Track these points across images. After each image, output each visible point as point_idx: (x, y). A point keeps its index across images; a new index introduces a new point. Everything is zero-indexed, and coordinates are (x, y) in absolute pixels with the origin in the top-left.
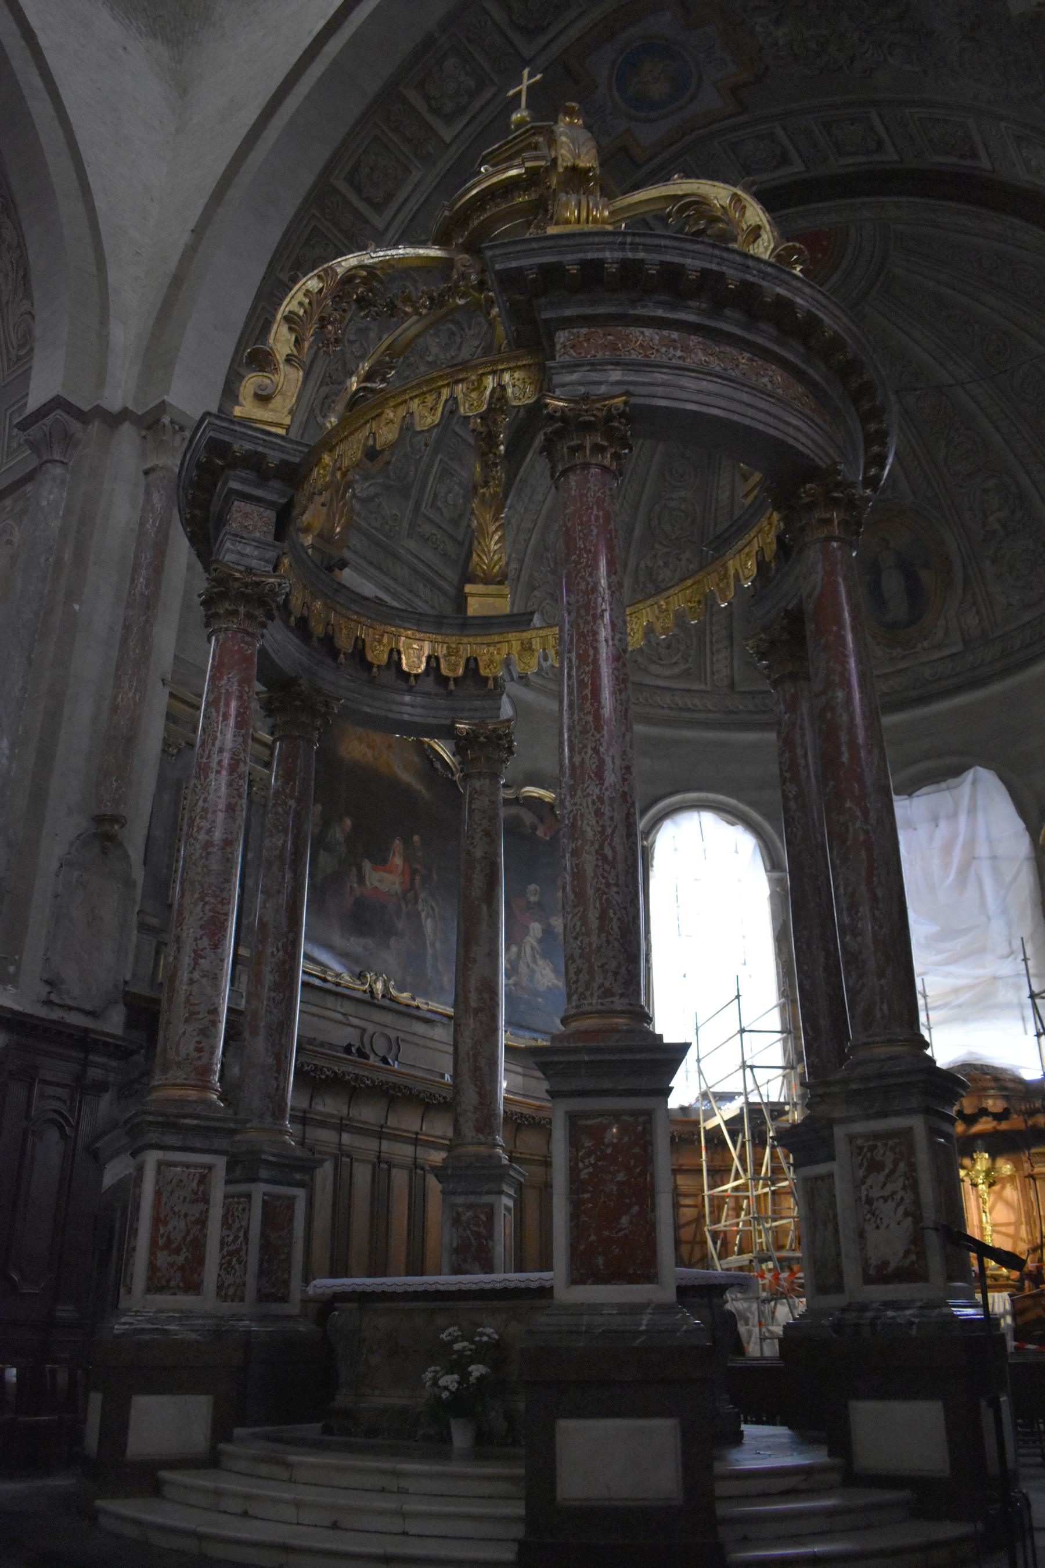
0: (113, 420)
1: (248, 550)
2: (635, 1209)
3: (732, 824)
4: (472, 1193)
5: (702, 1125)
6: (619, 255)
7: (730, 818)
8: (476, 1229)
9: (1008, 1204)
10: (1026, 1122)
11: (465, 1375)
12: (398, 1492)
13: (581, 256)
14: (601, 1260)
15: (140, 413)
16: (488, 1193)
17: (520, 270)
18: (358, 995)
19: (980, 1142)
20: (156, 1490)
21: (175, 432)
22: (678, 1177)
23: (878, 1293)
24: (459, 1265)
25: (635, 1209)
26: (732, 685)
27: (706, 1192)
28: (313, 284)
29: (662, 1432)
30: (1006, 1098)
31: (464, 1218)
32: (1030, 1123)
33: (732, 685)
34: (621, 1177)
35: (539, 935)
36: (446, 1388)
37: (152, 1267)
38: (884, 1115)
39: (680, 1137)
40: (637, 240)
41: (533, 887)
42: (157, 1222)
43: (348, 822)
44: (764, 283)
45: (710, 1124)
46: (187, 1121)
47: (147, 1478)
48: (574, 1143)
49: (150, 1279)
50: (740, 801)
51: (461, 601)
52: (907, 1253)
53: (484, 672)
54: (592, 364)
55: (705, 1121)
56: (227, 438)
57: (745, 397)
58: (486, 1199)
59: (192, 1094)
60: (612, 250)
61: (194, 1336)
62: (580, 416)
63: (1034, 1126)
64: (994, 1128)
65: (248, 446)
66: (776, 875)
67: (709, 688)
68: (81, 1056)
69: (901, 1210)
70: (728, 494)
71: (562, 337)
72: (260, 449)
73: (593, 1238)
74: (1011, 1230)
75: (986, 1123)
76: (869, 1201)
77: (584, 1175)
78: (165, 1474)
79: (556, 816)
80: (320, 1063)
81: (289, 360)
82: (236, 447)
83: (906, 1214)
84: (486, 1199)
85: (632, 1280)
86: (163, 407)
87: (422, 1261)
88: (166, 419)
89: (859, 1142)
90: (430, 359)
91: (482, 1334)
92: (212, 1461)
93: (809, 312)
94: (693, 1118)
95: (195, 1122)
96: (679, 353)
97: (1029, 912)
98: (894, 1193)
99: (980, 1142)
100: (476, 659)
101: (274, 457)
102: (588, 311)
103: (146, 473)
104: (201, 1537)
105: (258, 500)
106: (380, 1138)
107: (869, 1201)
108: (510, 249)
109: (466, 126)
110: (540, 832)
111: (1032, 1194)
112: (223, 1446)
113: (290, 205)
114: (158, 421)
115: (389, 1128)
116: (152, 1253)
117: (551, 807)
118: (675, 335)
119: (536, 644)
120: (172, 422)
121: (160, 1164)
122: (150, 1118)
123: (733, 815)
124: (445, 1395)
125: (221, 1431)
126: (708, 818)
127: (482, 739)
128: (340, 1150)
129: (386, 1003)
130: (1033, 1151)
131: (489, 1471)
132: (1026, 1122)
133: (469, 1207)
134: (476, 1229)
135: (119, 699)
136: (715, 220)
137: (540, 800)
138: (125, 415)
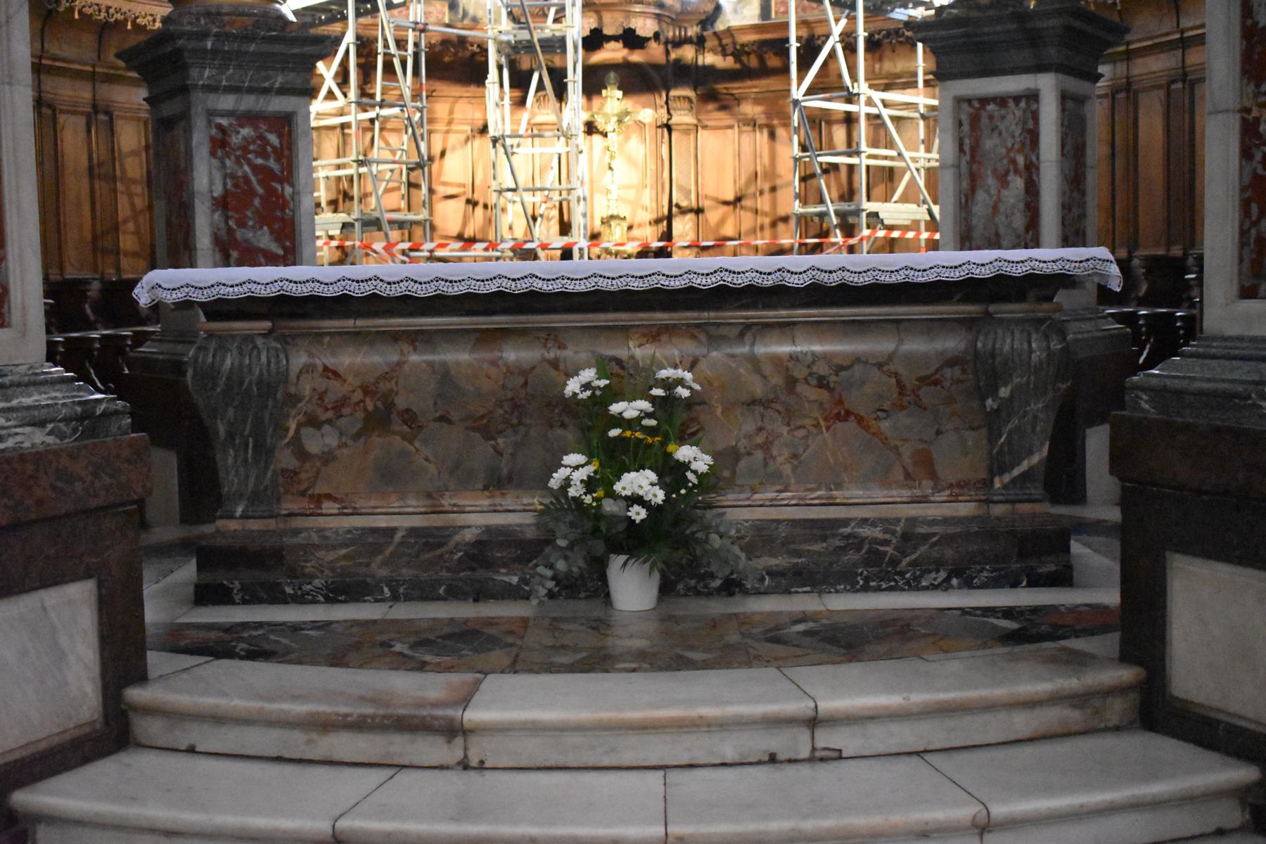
4: (251, 90)
8: (259, 161)
9: (631, 161)
10: (668, 53)
12: (811, 760)
16: (283, 91)
19: (612, 75)
24: (230, 231)
30: (658, 17)
31: (235, 140)
32: (673, 56)
36: (637, 500)
58: (278, 104)
61: (38, 438)
63: (678, 61)
64: (624, 58)
74: (631, 194)
75: (613, 50)
84: (278, 104)
87: (58, 214)
91: (669, 385)
92: (113, 733)
99: (612, 75)
111: (665, 150)
112: (136, 694)
130: (673, 93)
132: (668, 53)
133: (250, 118)
134: (259, 161)
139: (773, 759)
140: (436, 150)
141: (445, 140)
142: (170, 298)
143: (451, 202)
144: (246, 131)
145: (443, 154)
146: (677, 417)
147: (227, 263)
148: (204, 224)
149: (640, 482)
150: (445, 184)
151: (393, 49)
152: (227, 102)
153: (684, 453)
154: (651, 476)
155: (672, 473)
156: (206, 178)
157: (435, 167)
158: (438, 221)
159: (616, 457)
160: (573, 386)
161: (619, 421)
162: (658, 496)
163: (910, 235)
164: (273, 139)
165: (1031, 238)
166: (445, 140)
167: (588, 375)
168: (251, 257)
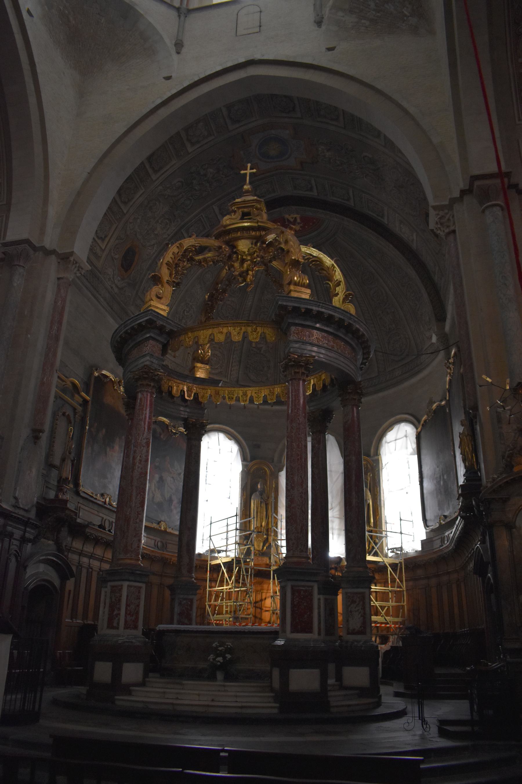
0: (48, 253)
1: (154, 361)
2: (308, 613)
3: (230, 439)
5: (209, 562)
6: (317, 309)
7: (230, 437)
11: (224, 658)
13: (306, 306)
14: (299, 627)
15: (60, 252)
17: (287, 306)
18: (100, 503)
20: (130, 693)
21: (73, 264)
22: (91, 560)
23: (351, 638)
25: (308, 613)
26: (237, 381)
27: (208, 589)
28: (176, 250)
29: (315, 673)
33: (237, 381)
34: (305, 604)
35: (158, 479)
36: (219, 661)
37: (126, 621)
38: (357, 588)
39: (200, 567)
40: (324, 305)
41: (157, 459)
42: (127, 605)
43: (104, 431)
44: (354, 324)
45: (214, 562)
46: (138, 572)
47: (127, 689)
48: (293, 594)
49: (125, 624)
50: (235, 430)
51: (193, 369)
52: (361, 627)
53: (200, 400)
54: (303, 342)
55: (210, 561)
56: (155, 319)
57: (342, 359)
58: (191, 597)
59: (133, 562)
60: (315, 307)
62: (300, 362)
65: (161, 323)
66: (245, 463)
67: (228, 381)
68: (23, 528)
69: (360, 615)
70: (250, 303)
71: (293, 328)
72: (164, 324)
73: (297, 621)
76: (351, 612)
77: (295, 603)
78: (132, 688)
79: (168, 430)
80: (103, 536)
81: (168, 282)
82: (158, 322)
83: (361, 616)
85: (307, 632)
86: (72, 253)
88: (72, 259)
89: (349, 595)
90: (156, 233)
91: (228, 645)
92: (143, 684)
93: (363, 333)
94: (206, 559)
95: (140, 572)
96: (326, 342)
97: (340, 494)
98: (358, 610)
100: (198, 394)
101: (168, 328)
102: (303, 323)
103: (59, 279)
104: (172, 704)
105: (157, 341)
106: (101, 562)
107: (351, 612)
108: (285, 298)
109: (198, 148)
110: (162, 436)
112: (147, 679)
113: (129, 171)
114: (68, 258)
115: (105, 558)
116: (126, 616)
117: (167, 426)
118: (326, 335)
119: (221, 393)
120: (74, 260)
121: (128, 586)
122: (127, 571)
123: (231, 436)
124: (219, 663)
125: (146, 675)
126: (222, 436)
127: (198, 426)
128: (100, 569)
129: (108, 507)
131: (252, 684)
135: (45, 380)
136: (323, 269)
137: (163, 422)
138: (53, 252)
139: (219, 691)
140: (264, 597)
141: (266, 595)
142: (161, 629)
143: (267, 613)
144: (185, 602)
145: (265, 599)
146: (229, 650)
147: (179, 624)
148: (176, 617)
149: (220, 659)
150: (266, 607)
151: (245, 573)
152: (182, 596)
153: (227, 655)
154: (222, 658)
155: (224, 658)
156: (177, 609)
157: (263, 602)
158: (263, 617)
159: (218, 656)
160: (214, 645)
161: (219, 650)
162: (222, 661)
163: (221, 622)
164: (189, 603)
165: (172, 623)
166: (266, 595)
167: (216, 643)
168: (183, 624)
